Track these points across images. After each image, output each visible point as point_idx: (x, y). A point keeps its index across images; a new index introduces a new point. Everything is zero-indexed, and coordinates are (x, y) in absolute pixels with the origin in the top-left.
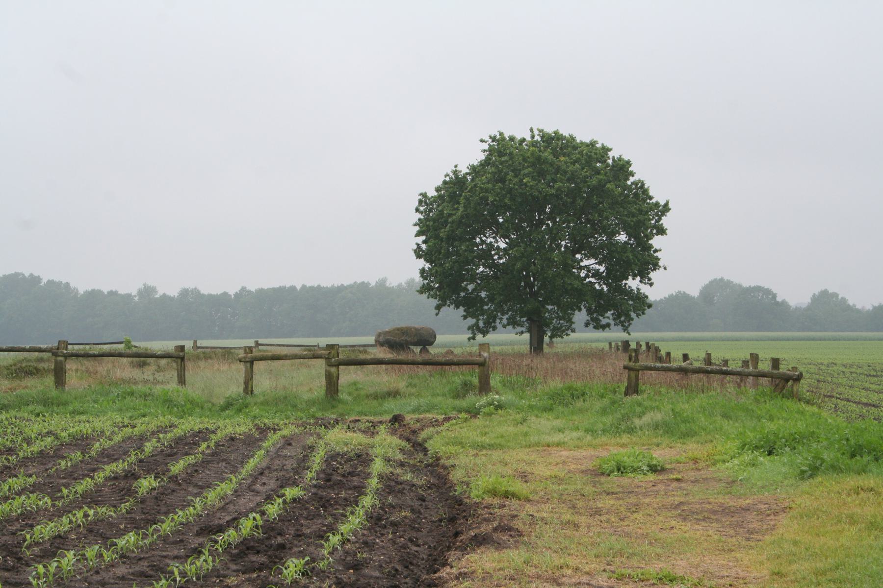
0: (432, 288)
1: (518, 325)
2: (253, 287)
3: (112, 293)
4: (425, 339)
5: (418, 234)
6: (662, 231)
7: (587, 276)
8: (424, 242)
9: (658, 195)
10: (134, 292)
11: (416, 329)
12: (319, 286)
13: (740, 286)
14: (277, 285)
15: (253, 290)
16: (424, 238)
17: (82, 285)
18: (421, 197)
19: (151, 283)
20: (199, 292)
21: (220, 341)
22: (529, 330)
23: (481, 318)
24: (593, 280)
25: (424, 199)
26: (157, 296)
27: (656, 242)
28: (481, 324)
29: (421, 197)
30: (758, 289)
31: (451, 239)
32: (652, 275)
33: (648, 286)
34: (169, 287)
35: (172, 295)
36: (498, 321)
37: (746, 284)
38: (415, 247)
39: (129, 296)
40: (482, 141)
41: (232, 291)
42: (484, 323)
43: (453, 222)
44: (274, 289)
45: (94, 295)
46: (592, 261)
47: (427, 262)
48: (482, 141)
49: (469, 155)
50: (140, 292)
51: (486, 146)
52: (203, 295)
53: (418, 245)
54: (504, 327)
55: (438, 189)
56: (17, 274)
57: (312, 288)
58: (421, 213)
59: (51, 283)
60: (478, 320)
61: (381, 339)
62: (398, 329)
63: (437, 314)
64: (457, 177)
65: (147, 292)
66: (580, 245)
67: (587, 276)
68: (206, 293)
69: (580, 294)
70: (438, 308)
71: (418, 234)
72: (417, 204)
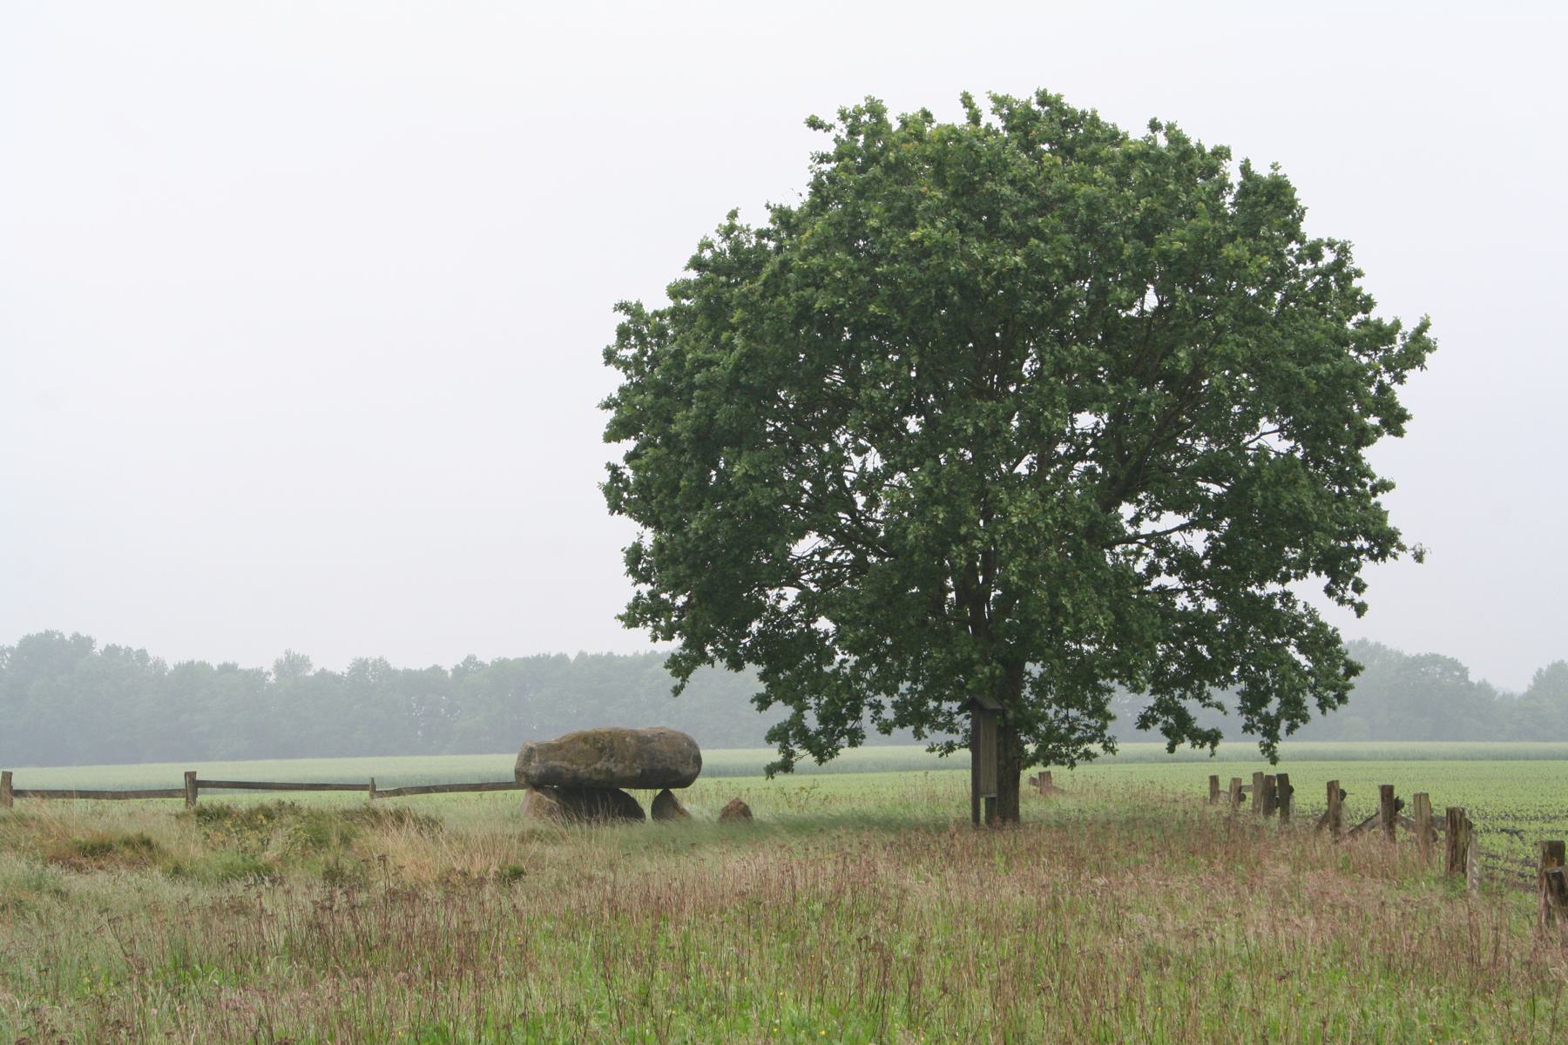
0: (667, 608)
1: (937, 726)
2: (487, 657)
3: (228, 669)
4: (669, 767)
5: (613, 435)
6: (1395, 420)
7: (1153, 570)
8: (630, 457)
9: (1392, 298)
10: (268, 667)
11: (642, 739)
12: (610, 654)
13: (1399, 655)
14: (531, 652)
15: (488, 662)
16: (630, 444)
17: (171, 651)
18: (624, 318)
19: (299, 650)
20: (387, 665)
21: (135, 767)
22: (973, 742)
23: (812, 701)
24: (1172, 582)
25: (635, 325)
26: (311, 673)
27: (1380, 456)
28: (812, 722)
29: (624, 318)
30: (1435, 659)
31: (707, 443)
32: (1368, 570)
33: (1349, 611)
34: (332, 657)
35: (339, 673)
36: (867, 713)
37: (1410, 651)
38: (606, 477)
39: (256, 676)
40: (814, 124)
41: (449, 662)
42: (823, 719)
43: (709, 385)
44: (526, 661)
45: (191, 673)
46: (1170, 520)
47: (646, 525)
48: (814, 124)
49: (770, 177)
50: (279, 667)
51: (826, 143)
52: (396, 672)
53: (613, 469)
54: (886, 729)
55: (676, 292)
56: (49, 635)
57: (597, 659)
58: (624, 365)
59: (112, 650)
60: (801, 709)
61: (534, 768)
62: (584, 738)
63: (677, 691)
64: (736, 249)
65: (292, 666)
66: (1134, 467)
67: (1153, 570)
68: (400, 668)
69: (1136, 626)
70: (681, 667)
71: (613, 435)
72: (612, 340)
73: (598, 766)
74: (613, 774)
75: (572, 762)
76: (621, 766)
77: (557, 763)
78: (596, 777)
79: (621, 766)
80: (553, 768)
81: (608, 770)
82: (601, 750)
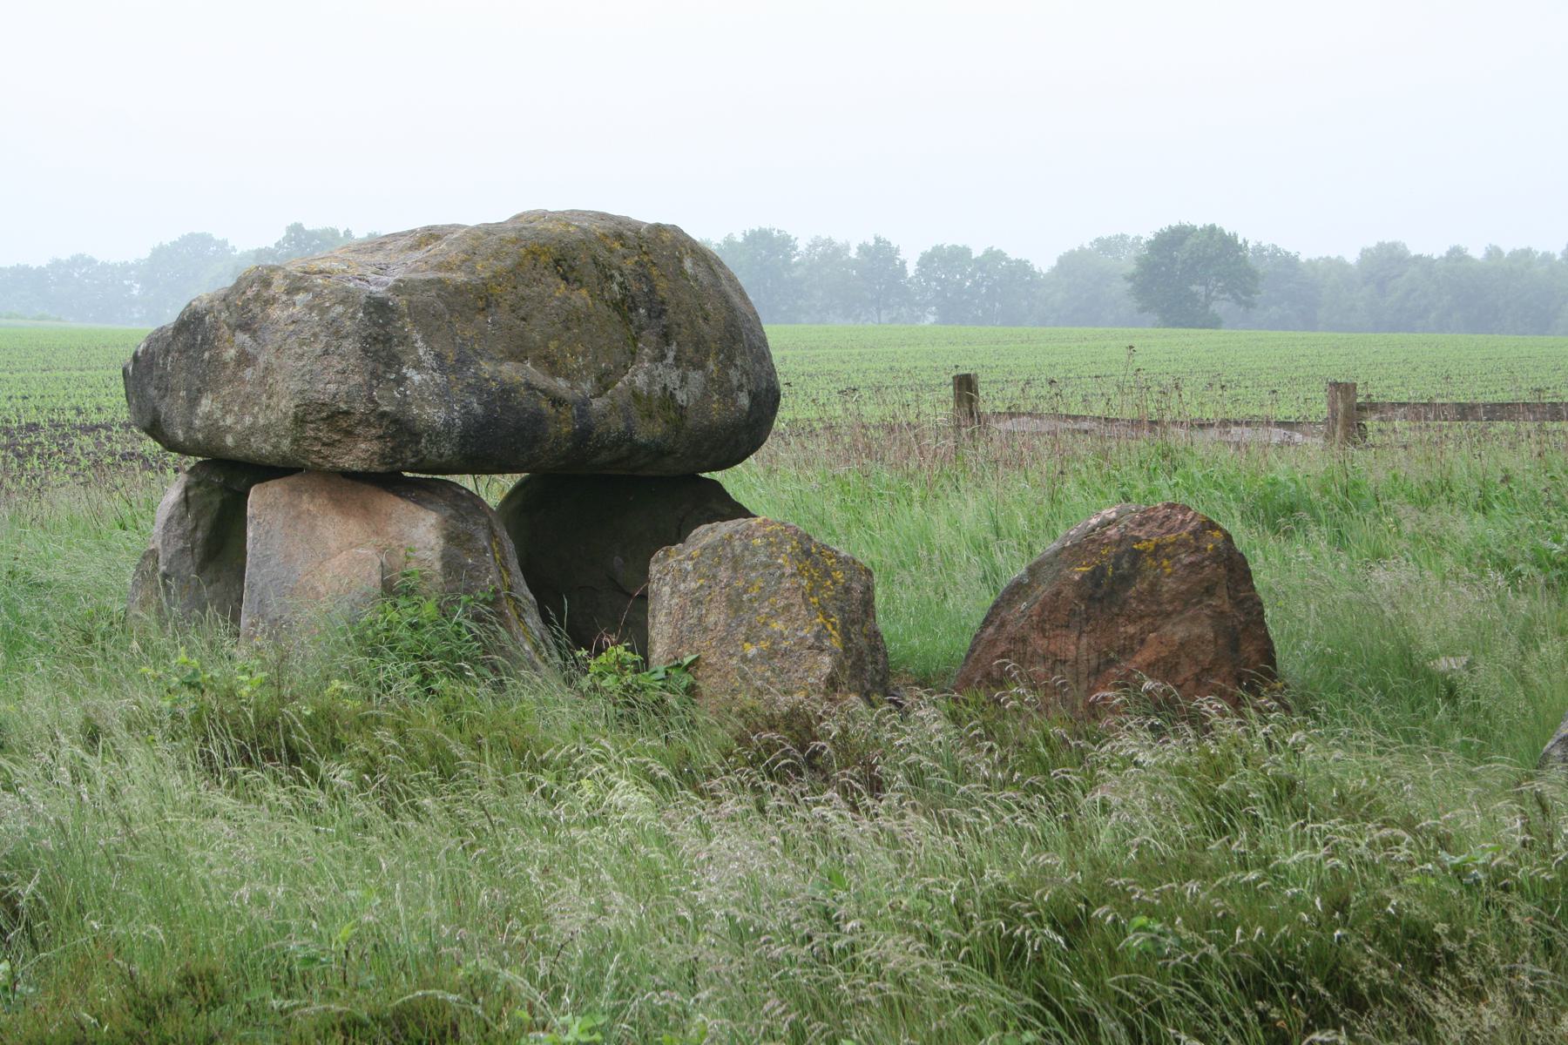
75: (551, 365)
80: (507, 391)
82: (624, 306)
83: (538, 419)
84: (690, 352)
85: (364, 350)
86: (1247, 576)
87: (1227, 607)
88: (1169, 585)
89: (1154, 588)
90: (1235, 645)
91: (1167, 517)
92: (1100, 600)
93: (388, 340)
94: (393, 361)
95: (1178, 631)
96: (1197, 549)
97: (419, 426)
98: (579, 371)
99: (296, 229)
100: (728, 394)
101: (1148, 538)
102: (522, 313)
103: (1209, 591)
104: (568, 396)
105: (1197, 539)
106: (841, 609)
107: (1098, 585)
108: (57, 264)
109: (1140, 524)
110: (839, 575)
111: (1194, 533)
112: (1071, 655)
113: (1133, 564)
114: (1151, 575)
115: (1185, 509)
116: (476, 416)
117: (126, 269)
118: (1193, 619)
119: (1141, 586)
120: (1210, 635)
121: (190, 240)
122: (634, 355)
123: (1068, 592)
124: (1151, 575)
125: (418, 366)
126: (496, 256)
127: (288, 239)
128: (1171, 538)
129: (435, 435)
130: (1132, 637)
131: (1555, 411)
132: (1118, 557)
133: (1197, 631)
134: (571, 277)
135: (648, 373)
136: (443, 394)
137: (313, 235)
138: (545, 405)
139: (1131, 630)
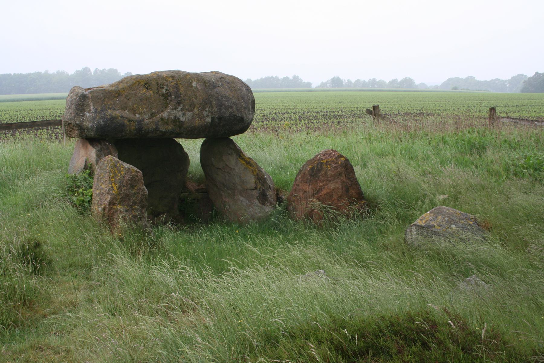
73: (165, 114)
74: (181, 124)
75: (135, 111)
76: (189, 115)
77: (117, 113)
78: (163, 129)
79: (189, 115)
80: (113, 118)
81: (176, 120)
82: (166, 97)
83: (123, 125)
84: (187, 107)
85: (76, 108)
86: (353, 171)
87: (345, 180)
88: (330, 173)
89: (326, 174)
90: (347, 190)
91: (331, 153)
92: (313, 176)
93: (83, 105)
94: (83, 110)
95: (332, 186)
96: (336, 163)
97: (84, 127)
98: (144, 112)
99: (537, 73)
100: (202, 117)
101: (324, 160)
102: (128, 98)
103: (340, 175)
104: (134, 119)
105: (336, 160)
106: (120, 182)
107: (313, 172)
108: (492, 80)
109: (324, 155)
110: (123, 173)
111: (336, 158)
112: (307, 190)
113: (321, 166)
114: (325, 169)
115: (335, 151)
116: (101, 125)
117: (506, 81)
118: (336, 182)
119: (323, 172)
120: (341, 187)
121: (519, 75)
122: (166, 108)
123: (307, 173)
124: (325, 169)
125: (89, 112)
126: (126, 83)
127: (535, 75)
128: (330, 159)
129: (88, 130)
130: (321, 186)
131: (540, 120)
132: (318, 164)
133: (337, 186)
134: (149, 88)
135: (169, 113)
136: (94, 119)
137: (540, 74)
138: (126, 122)
139: (321, 184)
